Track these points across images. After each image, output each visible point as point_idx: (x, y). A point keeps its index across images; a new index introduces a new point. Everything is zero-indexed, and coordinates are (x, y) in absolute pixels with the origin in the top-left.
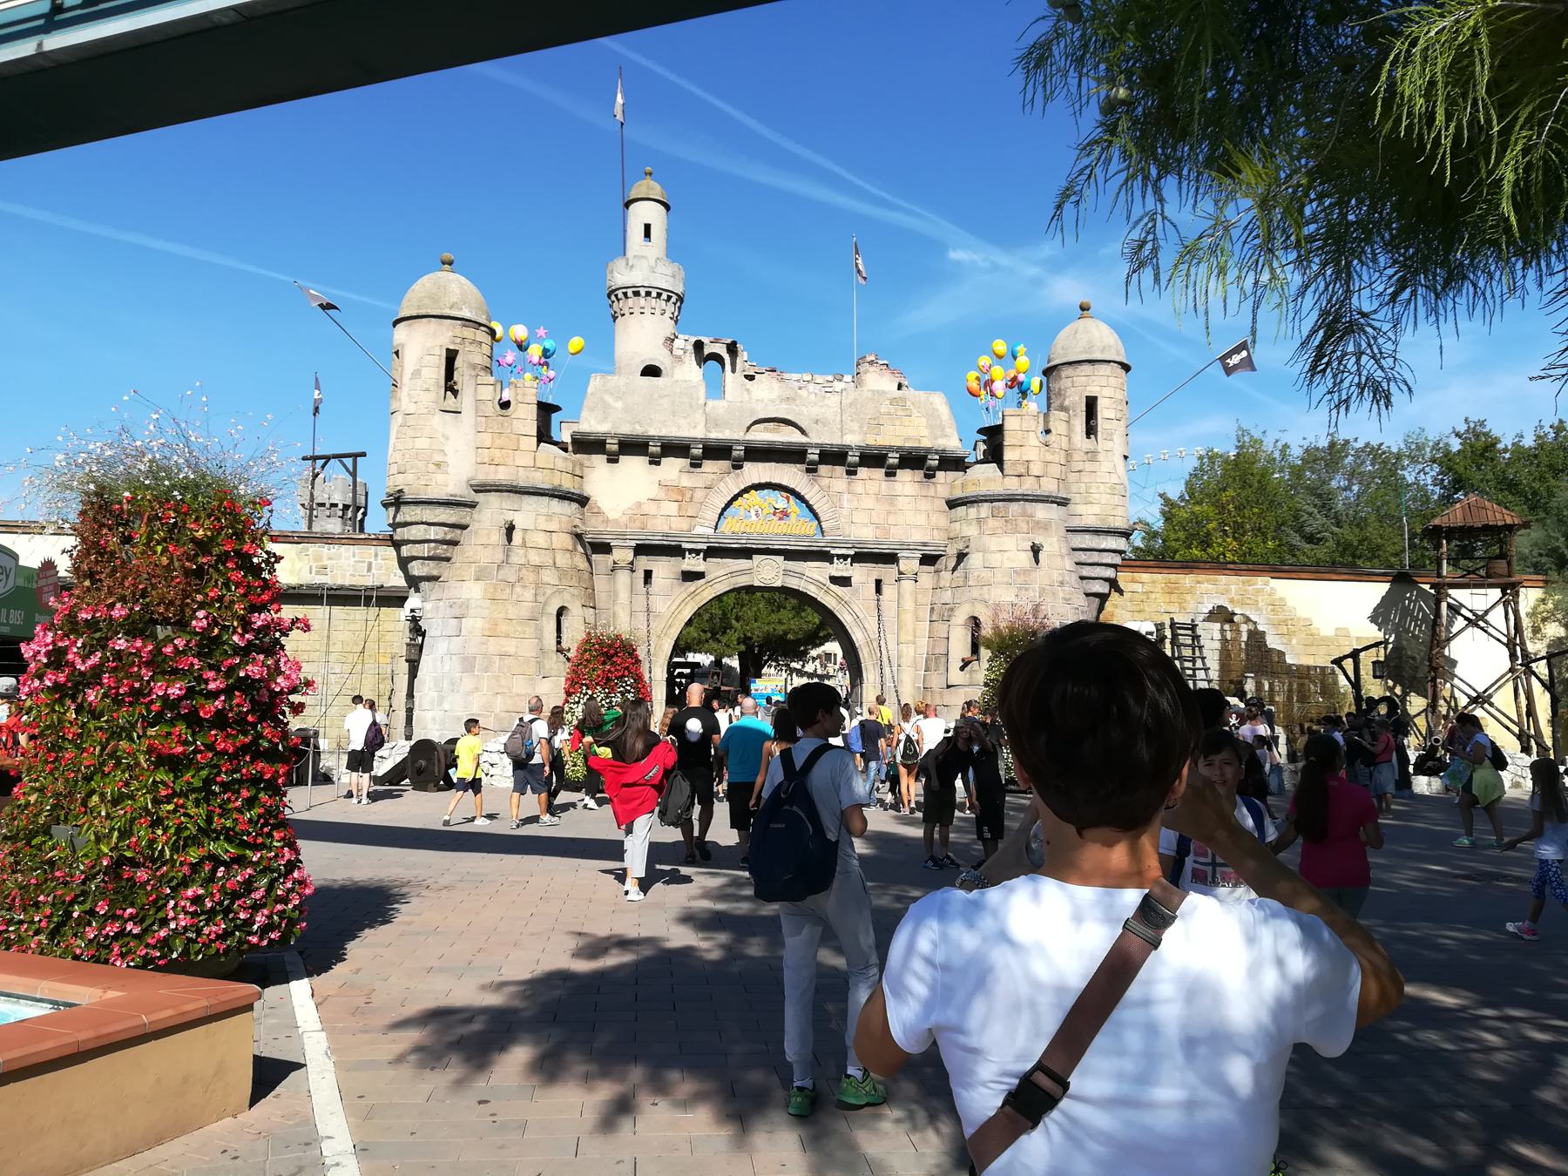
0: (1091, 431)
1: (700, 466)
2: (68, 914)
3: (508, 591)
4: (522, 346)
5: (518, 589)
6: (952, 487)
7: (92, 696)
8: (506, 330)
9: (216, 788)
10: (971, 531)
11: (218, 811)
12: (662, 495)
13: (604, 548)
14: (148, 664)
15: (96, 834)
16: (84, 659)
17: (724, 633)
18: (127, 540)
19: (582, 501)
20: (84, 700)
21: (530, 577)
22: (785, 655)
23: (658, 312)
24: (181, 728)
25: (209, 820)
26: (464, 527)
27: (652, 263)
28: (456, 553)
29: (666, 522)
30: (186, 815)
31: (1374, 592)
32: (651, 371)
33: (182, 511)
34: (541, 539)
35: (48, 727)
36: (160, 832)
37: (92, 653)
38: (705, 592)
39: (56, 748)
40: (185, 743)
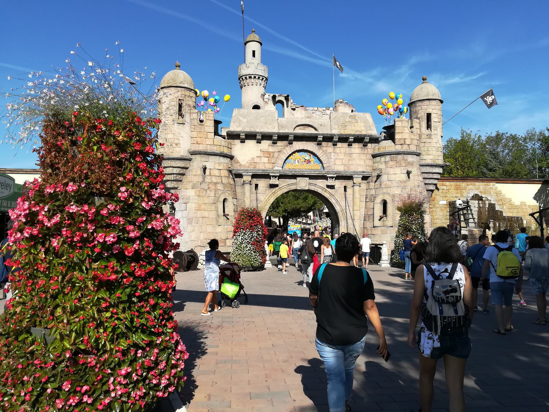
0: (429, 126)
1: (276, 143)
2: (44, 390)
3: (205, 192)
4: (206, 99)
5: (208, 192)
6: (374, 149)
7: (55, 243)
8: (200, 92)
9: (135, 300)
10: (382, 166)
11: (137, 314)
13: (240, 176)
14: (92, 222)
15: (60, 334)
16: (50, 219)
17: (278, 208)
18: (74, 143)
19: (231, 158)
20: (50, 245)
21: (212, 187)
22: (296, 217)
23: (258, 84)
24: (114, 263)
25: (132, 321)
26: (187, 168)
27: (256, 65)
28: (184, 178)
29: (263, 165)
30: (118, 319)
31: (535, 188)
32: (256, 107)
33: (110, 125)
34: (216, 173)
35: (27, 264)
36: (101, 331)
37: (54, 215)
38: (279, 192)
39: (32, 276)
40: (117, 272)
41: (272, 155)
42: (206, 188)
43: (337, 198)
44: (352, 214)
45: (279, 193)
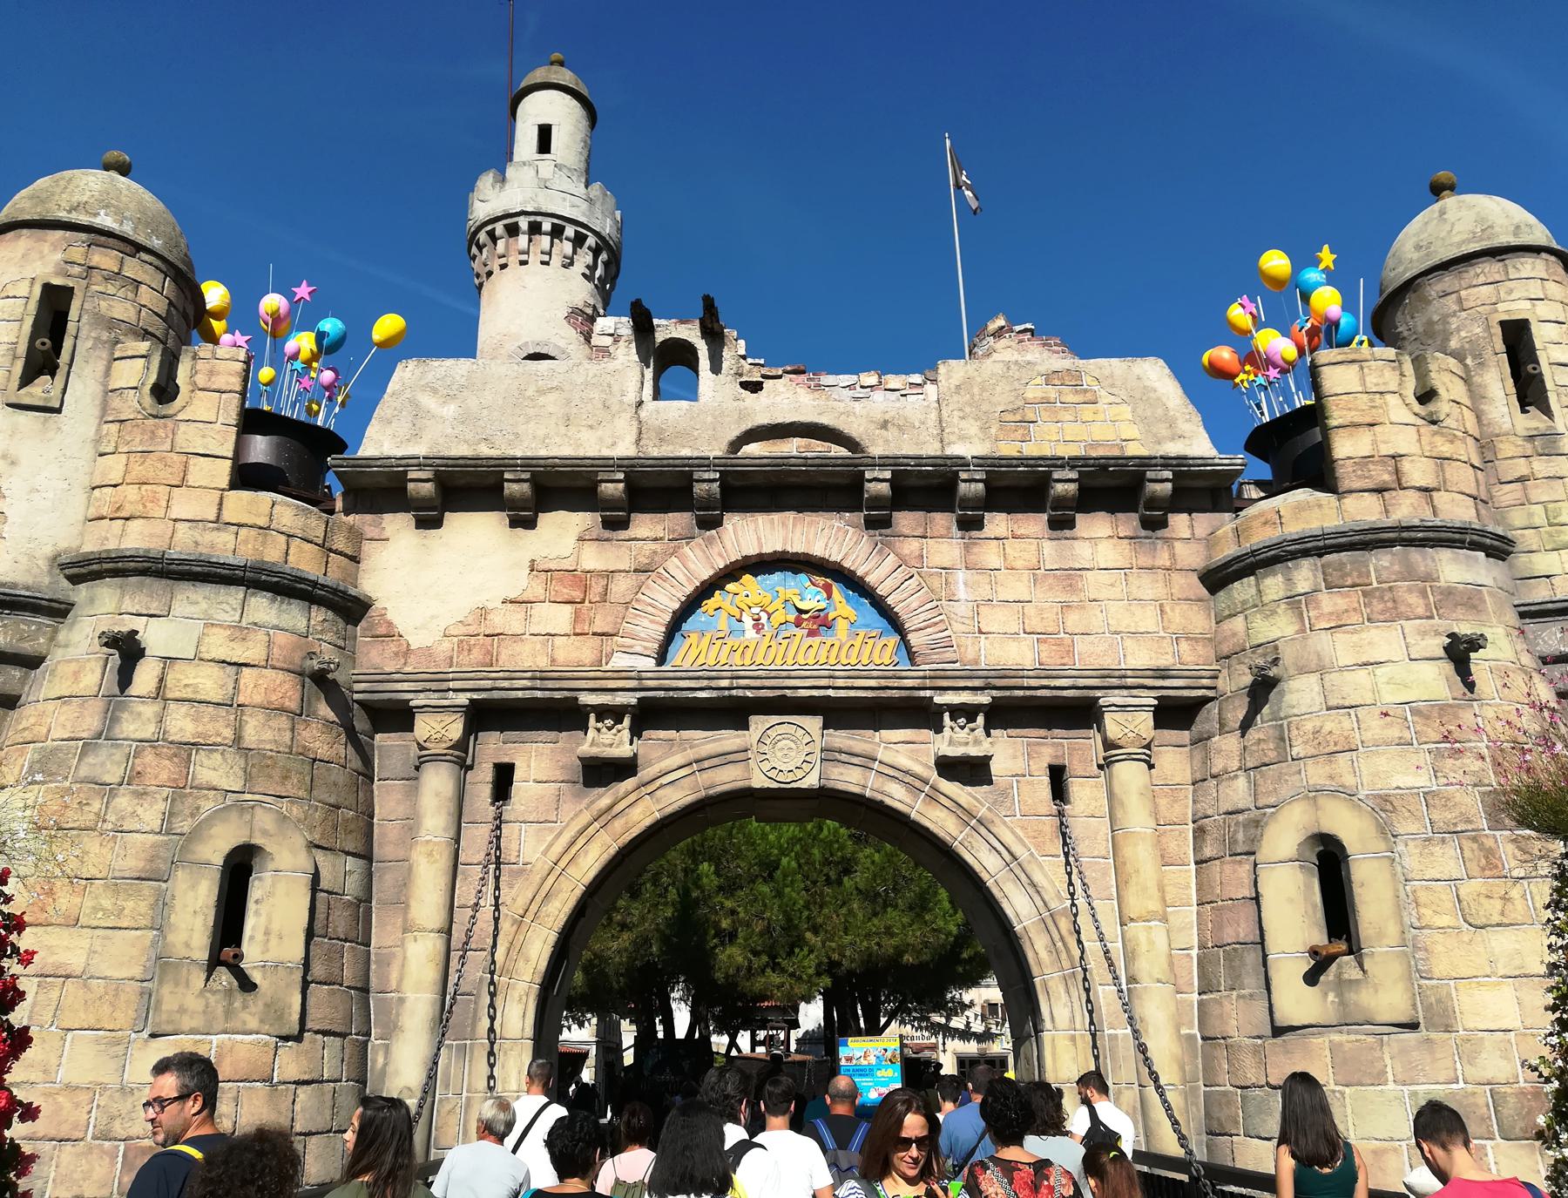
0: (1530, 391)
1: (624, 524)
5: (123, 801)
6: (1210, 540)
10: (1277, 627)
13: (397, 716)
17: (790, 953)
19: (351, 609)
21: (160, 769)
26: (32, 662)
29: (546, 645)
34: (209, 682)
41: (597, 588)
43: (1008, 838)
44: (1116, 948)
45: (642, 815)
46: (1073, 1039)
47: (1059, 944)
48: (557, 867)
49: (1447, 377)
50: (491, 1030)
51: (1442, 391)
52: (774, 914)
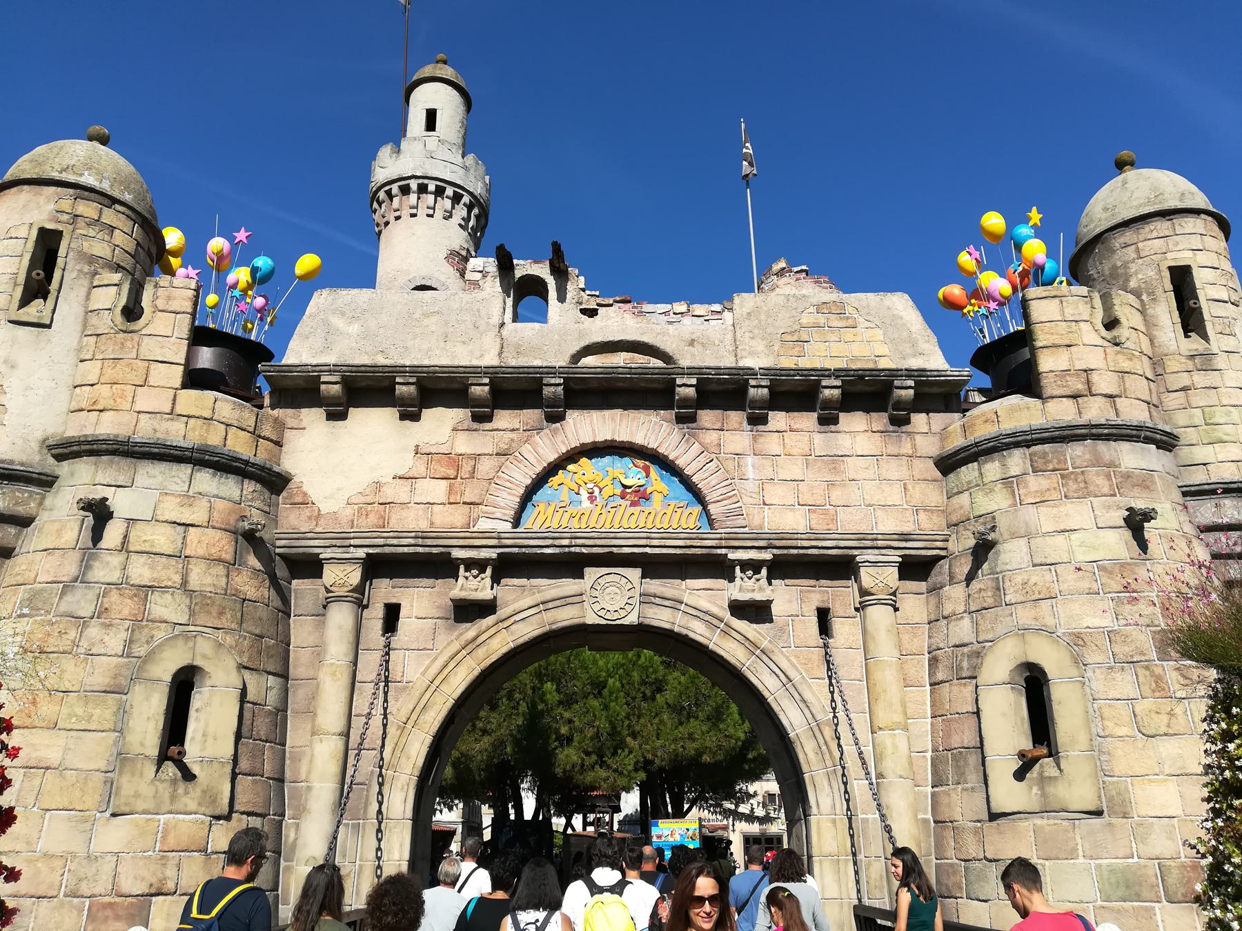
0: (1191, 320)
1: (488, 418)
5: (94, 631)
6: (943, 434)
10: (994, 502)
12: (421, 469)
13: (309, 566)
17: (614, 754)
21: (122, 606)
26: (24, 522)
29: (425, 513)
34: (163, 539)
38: (497, 640)
41: (466, 467)
42: (86, 610)
43: (785, 665)
44: (868, 751)
46: (834, 821)
47: (824, 748)
48: (434, 685)
49: (1127, 309)
50: (380, 812)
51: (1123, 320)
52: (603, 724)
